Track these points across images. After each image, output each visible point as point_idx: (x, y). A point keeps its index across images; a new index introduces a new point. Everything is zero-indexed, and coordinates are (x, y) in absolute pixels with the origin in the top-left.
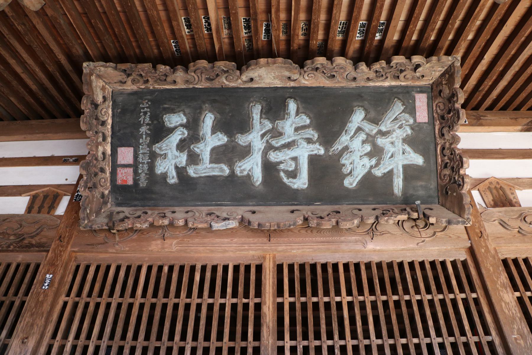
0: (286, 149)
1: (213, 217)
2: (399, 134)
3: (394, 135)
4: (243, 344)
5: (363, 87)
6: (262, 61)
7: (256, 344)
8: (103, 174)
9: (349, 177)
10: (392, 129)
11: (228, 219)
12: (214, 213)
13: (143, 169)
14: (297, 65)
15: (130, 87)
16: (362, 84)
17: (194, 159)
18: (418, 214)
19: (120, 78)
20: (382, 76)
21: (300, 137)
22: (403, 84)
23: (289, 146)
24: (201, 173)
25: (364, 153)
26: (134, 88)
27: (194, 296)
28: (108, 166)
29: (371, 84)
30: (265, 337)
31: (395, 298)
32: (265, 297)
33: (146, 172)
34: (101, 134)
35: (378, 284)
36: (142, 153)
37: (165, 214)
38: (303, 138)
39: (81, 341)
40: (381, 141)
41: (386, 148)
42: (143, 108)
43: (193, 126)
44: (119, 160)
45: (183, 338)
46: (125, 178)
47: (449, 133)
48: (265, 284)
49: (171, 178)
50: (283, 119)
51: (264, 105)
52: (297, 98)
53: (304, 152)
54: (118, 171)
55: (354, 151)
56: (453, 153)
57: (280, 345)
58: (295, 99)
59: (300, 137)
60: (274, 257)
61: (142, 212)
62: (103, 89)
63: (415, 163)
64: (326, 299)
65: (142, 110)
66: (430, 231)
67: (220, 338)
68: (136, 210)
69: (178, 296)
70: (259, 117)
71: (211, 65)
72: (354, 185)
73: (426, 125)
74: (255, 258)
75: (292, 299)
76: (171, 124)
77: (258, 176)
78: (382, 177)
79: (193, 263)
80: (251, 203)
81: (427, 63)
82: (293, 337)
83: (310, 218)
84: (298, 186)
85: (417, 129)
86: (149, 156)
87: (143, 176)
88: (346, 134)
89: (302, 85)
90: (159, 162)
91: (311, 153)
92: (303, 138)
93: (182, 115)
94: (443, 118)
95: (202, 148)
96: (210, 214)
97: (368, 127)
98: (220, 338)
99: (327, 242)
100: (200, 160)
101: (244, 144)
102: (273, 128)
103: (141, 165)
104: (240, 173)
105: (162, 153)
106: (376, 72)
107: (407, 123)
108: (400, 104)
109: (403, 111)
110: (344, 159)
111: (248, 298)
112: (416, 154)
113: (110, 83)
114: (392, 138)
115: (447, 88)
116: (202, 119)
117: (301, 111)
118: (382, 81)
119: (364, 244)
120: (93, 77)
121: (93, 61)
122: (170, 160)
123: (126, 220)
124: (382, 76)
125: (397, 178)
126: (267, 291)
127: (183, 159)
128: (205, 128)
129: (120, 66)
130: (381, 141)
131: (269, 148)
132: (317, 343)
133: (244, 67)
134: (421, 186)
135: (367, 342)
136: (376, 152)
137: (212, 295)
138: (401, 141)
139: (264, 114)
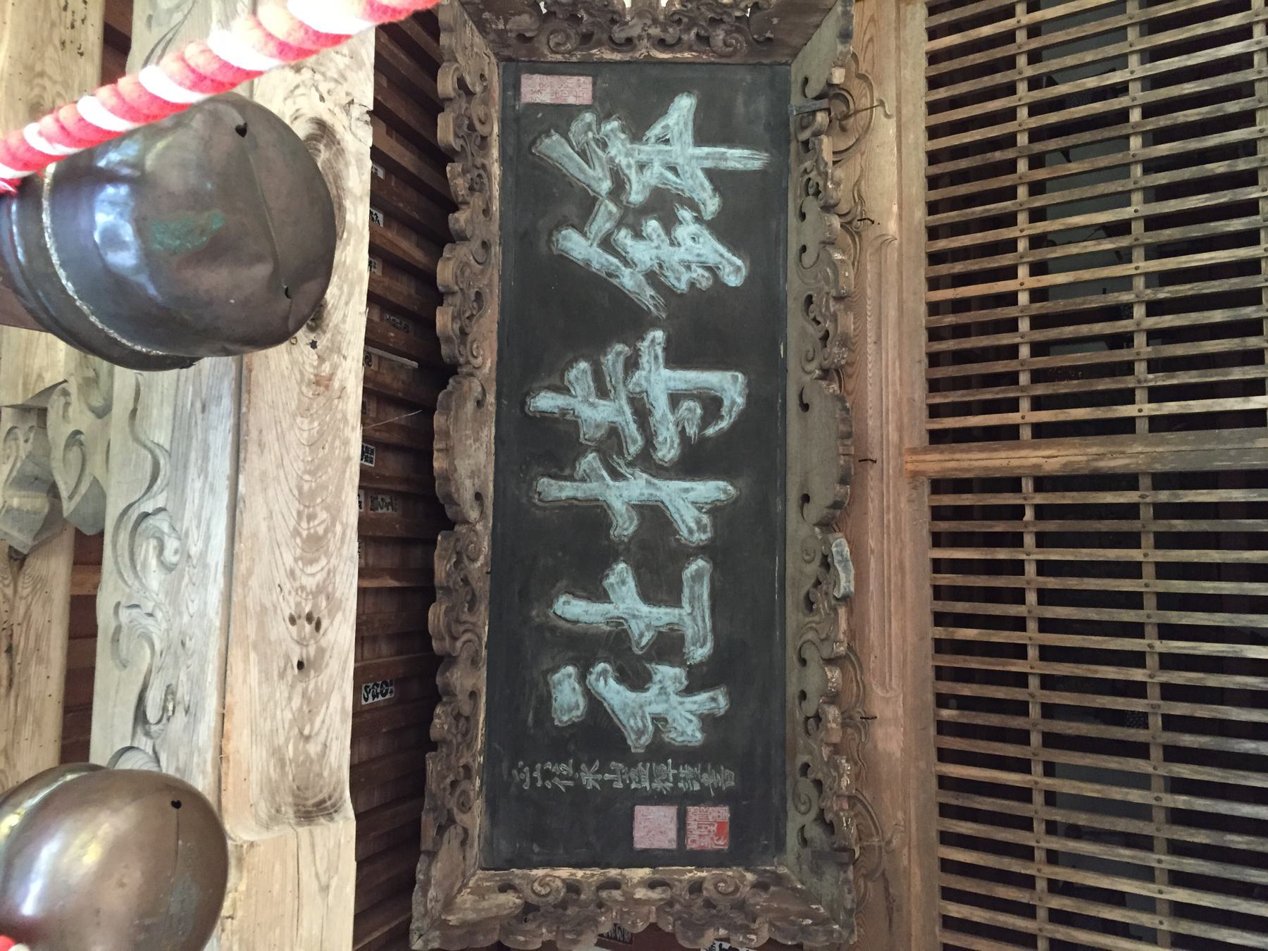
0: (651, 419)
1: (818, 595)
2: (620, 150)
3: (622, 161)
4: (1146, 513)
5: (500, 229)
6: (439, 463)
7: (1145, 482)
8: (706, 885)
9: (721, 273)
10: (607, 167)
11: (825, 557)
12: (808, 594)
13: (690, 778)
14: (451, 381)
15: (475, 819)
16: (495, 227)
17: (669, 646)
18: (820, 110)
19: (456, 843)
20: (479, 176)
21: (620, 387)
22: (496, 130)
23: (642, 412)
24: (705, 627)
25: (663, 236)
26: (478, 805)
27: (1019, 638)
28: (684, 873)
29: (496, 206)
30: (1127, 461)
31: (1022, 166)
32: (1019, 467)
33: (697, 771)
34: (604, 894)
35: (987, 207)
36: (651, 782)
37: (807, 718)
38: (625, 379)
39: (1161, 923)
40: (637, 193)
41: (653, 182)
42: (534, 780)
43: (586, 648)
44: (666, 845)
45: (1137, 659)
46: (714, 828)
47: (627, 23)
48: (986, 469)
49: (713, 705)
50: (575, 425)
51: (541, 469)
52: (525, 391)
53: (659, 380)
54: (694, 846)
55: (658, 258)
56: (676, 17)
57: (1147, 426)
58: (527, 394)
59: (620, 387)
60: (913, 451)
61: (803, 779)
62: (480, 893)
63: (691, 117)
64: (1024, 325)
65: (539, 784)
66: (857, 87)
67: (1133, 570)
68: (796, 796)
69: (1020, 680)
70: (569, 483)
71: (439, 594)
72: (739, 262)
73: (599, 81)
74: (915, 495)
75: (1025, 405)
76: (577, 706)
77: (710, 490)
78: (722, 195)
79: (929, 646)
80: (780, 507)
81: (456, 61)
82: (1127, 397)
83: (826, 364)
84: (740, 395)
85: (608, 105)
86: (658, 763)
87: (707, 779)
88: (617, 277)
89: (494, 375)
90: (673, 735)
91: (661, 360)
92: (625, 379)
93: (557, 676)
94: (586, 39)
95: (642, 626)
96: (809, 604)
97: (601, 223)
98: (1133, 570)
99: (880, 328)
100: (672, 630)
101: (636, 522)
102: (598, 450)
103: (681, 785)
104: (705, 532)
105: (651, 728)
106: (471, 189)
107: (594, 127)
108: (547, 141)
109: (565, 135)
110: (676, 284)
111: (1022, 507)
112: (671, 111)
113: (464, 875)
114: (629, 166)
115: (517, 18)
116: (569, 625)
117: (558, 383)
118: (490, 179)
119: (884, 242)
120: (453, 919)
121: (409, 921)
122: (672, 707)
123: (829, 817)
124: (479, 176)
125: (726, 159)
126: (1005, 463)
127: (668, 674)
128: (592, 619)
129: (426, 844)
130: (637, 193)
131: (646, 461)
132: (1140, 340)
133: (450, 513)
134: (746, 104)
135: (1137, 227)
136: (664, 206)
137: (1017, 596)
138: (636, 146)
139: (562, 469)
